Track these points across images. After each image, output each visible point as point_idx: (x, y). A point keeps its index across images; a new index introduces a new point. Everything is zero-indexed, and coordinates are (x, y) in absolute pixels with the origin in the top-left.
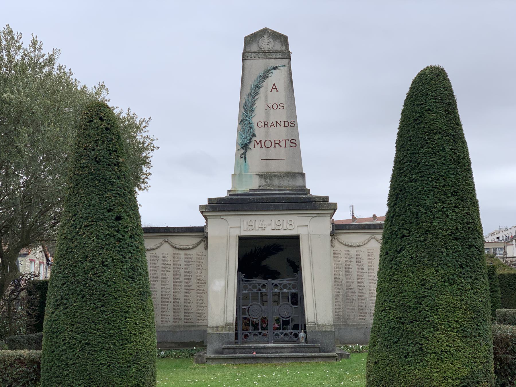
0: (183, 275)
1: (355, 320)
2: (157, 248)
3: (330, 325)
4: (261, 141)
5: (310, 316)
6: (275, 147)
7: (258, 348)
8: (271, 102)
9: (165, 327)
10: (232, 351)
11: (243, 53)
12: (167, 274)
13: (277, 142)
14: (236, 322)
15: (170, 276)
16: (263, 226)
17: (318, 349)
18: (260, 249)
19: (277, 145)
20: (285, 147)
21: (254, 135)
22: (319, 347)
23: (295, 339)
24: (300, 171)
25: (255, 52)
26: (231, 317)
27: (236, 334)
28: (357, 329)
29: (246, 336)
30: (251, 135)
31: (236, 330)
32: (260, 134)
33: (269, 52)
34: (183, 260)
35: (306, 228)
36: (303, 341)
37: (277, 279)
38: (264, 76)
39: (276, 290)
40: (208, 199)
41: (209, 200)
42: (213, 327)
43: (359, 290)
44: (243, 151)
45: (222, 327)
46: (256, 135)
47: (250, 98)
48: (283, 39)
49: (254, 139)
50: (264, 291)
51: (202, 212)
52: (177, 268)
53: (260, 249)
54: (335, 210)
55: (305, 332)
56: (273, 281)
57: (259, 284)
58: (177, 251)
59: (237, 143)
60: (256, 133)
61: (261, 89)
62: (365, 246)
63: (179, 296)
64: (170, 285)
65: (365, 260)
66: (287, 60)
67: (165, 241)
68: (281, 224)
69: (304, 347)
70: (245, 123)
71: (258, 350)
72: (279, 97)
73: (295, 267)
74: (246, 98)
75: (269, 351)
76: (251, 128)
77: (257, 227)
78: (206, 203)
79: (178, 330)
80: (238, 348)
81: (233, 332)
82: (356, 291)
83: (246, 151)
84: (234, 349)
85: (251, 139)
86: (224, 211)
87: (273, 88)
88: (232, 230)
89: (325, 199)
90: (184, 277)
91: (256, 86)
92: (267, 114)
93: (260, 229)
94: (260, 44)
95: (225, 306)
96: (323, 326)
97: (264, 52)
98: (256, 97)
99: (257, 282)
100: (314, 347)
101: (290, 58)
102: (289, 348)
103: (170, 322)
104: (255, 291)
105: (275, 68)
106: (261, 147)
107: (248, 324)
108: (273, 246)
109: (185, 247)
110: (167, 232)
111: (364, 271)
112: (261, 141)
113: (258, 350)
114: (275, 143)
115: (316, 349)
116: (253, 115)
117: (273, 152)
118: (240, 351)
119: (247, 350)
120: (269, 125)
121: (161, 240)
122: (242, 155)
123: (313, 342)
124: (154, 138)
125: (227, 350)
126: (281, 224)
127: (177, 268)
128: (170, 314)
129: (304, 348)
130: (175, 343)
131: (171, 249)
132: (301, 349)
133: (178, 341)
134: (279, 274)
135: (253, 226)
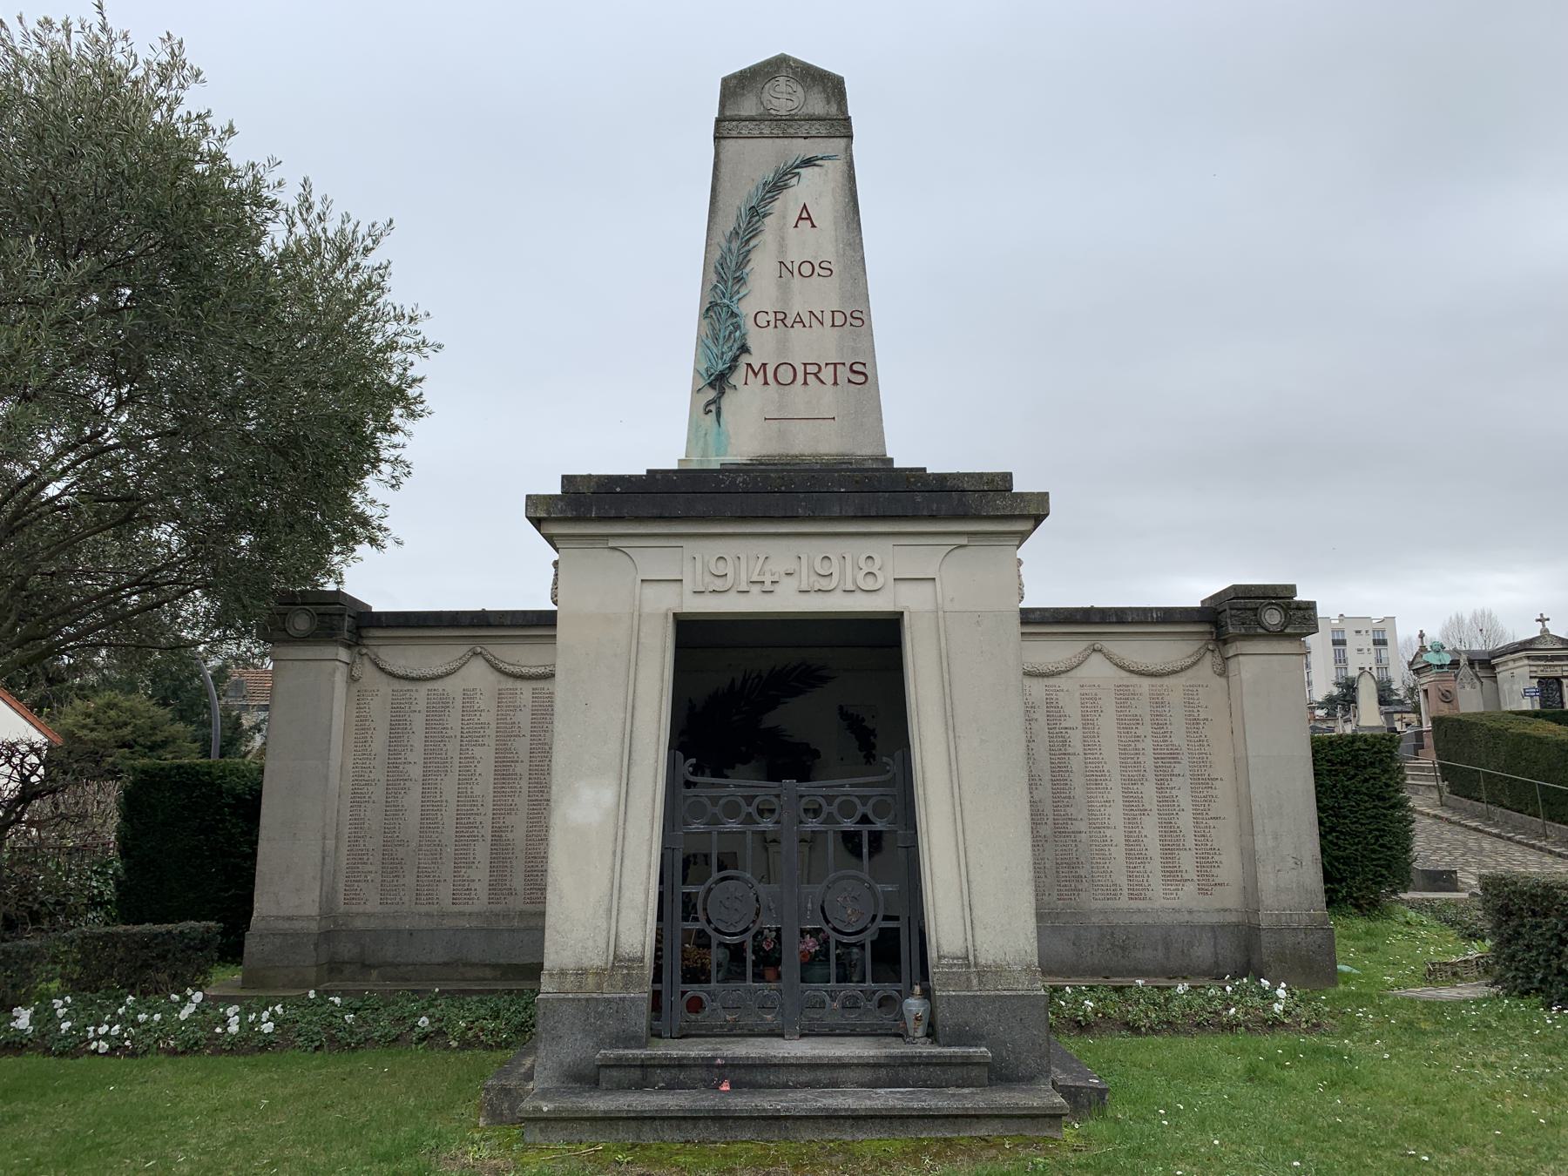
0: (524, 754)
2: (447, 674)
5: (944, 930)
6: (805, 383)
8: (794, 256)
9: (462, 914)
10: (636, 1074)
11: (718, 121)
12: (478, 752)
14: (657, 958)
15: (485, 757)
16: (768, 579)
18: (759, 676)
19: (810, 378)
20: (835, 383)
21: (744, 349)
23: (887, 1019)
24: (876, 451)
25: (752, 119)
26: (638, 932)
27: (656, 995)
29: (695, 1005)
31: (657, 978)
32: (763, 346)
33: (791, 119)
36: (920, 1033)
37: (808, 780)
38: (777, 186)
39: (812, 824)
41: (567, 480)
42: (563, 973)
44: (711, 394)
45: (599, 973)
47: (735, 245)
48: (833, 87)
49: (745, 359)
50: (767, 824)
51: (537, 522)
52: (507, 733)
53: (759, 676)
54: (1038, 519)
55: (927, 994)
56: (803, 788)
57: (749, 799)
58: (510, 684)
59: (696, 371)
60: (750, 343)
61: (766, 220)
63: (509, 820)
64: (484, 786)
65: (1074, 717)
66: (842, 142)
67: (475, 654)
68: (835, 570)
69: (929, 1062)
70: (720, 313)
71: (747, 1075)
72: (821, 243)
74: (724, 244)
75: (783, 1078)
76: (737, 327)
77: (744, 577)
78: (556, 490)
79: (504, 924)
80: (661, 1066)
81: (642, 993)
82: (1049, 810)
83: (722, 393)
84: (644, 1065)
85: (735, 359)
86: (619, 519)
87: (800, 218)
88: (650, 590)
89: (1002, 482)
91: (754, 211)
92: (784, 290)
93: (755, 589)
94: (766, 96)
95: (616, 889)
96: (998, 971)
97: (777, 120)
98: (752, 243)
100: (967, 1062)
101: (851, 137)
102: (867, 1065)
103: (480, 900)
104: (733, 825)
105: (808, 162)
106: (766, 383)
107: (704, 952)
108: (795, 668)
109: (533, 670)
110: (479, 626)
111: (1070, 750)
116: (743, 291)
117: (800, 398)
118: (667, 1075)
119: (698, 1074)
120: (789, 322)
121: (462, 650)
122: (708, 404)
123: (960, 1038)
124: (420, 312)
126: (835, 570)
127: (507, 733)
128: (480, 876)
130: (495, 966)
131: (493, 677)
132: (914, 1071)
133: (501, 961)
134: (816, 754)
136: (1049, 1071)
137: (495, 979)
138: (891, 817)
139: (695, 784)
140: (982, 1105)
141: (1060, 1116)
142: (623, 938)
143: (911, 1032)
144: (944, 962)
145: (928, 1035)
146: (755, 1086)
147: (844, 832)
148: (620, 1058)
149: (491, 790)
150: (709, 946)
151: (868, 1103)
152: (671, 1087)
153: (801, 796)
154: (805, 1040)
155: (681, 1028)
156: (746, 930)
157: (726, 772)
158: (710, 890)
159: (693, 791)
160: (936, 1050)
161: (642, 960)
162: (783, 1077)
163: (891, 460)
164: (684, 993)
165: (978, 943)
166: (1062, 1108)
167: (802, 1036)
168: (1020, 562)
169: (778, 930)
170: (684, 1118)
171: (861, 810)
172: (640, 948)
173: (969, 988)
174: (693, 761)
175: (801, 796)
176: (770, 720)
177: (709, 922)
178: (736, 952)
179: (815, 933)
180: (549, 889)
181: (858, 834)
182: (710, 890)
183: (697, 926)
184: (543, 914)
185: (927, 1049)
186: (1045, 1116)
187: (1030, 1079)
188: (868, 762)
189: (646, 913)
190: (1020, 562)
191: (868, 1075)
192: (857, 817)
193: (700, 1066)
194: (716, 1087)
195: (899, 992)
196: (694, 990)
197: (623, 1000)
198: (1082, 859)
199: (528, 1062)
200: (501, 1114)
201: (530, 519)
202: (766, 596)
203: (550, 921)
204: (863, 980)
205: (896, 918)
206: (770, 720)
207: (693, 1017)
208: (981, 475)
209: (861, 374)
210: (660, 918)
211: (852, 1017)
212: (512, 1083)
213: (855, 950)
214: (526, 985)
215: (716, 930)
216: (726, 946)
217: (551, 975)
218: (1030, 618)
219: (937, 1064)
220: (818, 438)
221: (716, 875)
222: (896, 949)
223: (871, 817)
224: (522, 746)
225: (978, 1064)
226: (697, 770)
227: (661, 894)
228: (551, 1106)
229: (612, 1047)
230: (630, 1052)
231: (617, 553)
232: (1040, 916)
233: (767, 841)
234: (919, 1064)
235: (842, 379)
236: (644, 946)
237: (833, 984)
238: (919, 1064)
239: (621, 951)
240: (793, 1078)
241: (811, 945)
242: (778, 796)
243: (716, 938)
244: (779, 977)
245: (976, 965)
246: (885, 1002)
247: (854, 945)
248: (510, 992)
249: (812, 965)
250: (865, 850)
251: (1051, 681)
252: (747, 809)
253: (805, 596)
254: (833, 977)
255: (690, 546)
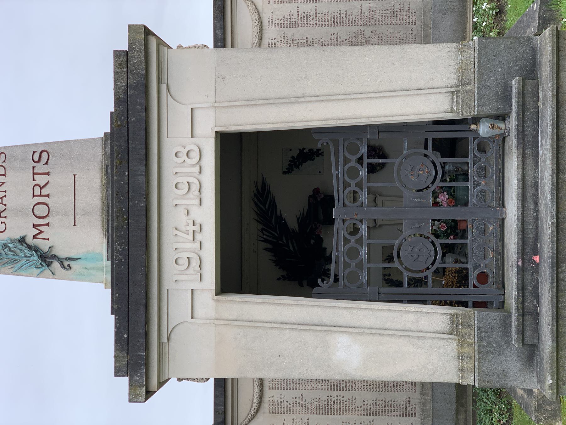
1: (414, 33)
3: (461, 51)
4: (34, 226)
5: (432, 106)
6: (48, 196)
7: (523, 249)
10: (529, 320)
13: (37, 192)
14: (451, 304)
16: (191, 228)
17: (529, 82)
19: (44, 192)
20: (48, 174)
21: (22, 240)
22: (523, 81)
23: (492, 148)
26: (433, 318)
27: (476, 305)
28: (434, 28)
29: (483, 278)
30: (20, 247)
31: (464, 304)
34: (285, 392)
35: (198, 115)
36: (502, 125)
37: (333, 197)
39: (363, 197)
40: (116, 375)
41: (118, 372)
42: (461, 370)
43: (353, 24)
44: (56, 265)
45: (461, 344)
46: (23, 235)
49: (29, 240)
50: (363, 229)
51: (149, 394)
54: (148, 32)
55: (476, 120)
56: (338, 204)
57: (346, 241)
58: (265, 405)
59: (38, 275)
60: (18, 236)
62: (260, 9)
63: (359, 403)
69: (522, 121)
73: (302, 149)
77: (189, 245)
79: (429, 406)
80: (523, 303)
81: (475, 315)
82: (355, 29)
83: (55, 257)
84: (523, 313)
85: (29, 247)
88: (199, 312)
89: (122, 59)
90: (320, 392)
93: (199, 237)
95: (404, 333)
96: (462, 71)
99: (341, 248)
100: (522, 94)
104: (363, 253)
106: (48, 225)
107: (450, 273)
108: (256, 204)
111: (313, 13)
112: (34, 226)
113: (529, 249)
114: (41, 195)
115: (529, 89)
117: (59, 199)
119: (528, 278)
122: (64, 267)
123: (506, 98)
125: (528, 333)
129: (523, 121)
130: (457, 412)
131: (260, 418)
132: (528, 130)
133: (454, 407)
134: (316, 191)
135: (190, 255)
136: (529, 38)
137: (466, 412)
138: (358, 143)
139: (336, 276)
140: (550, 85)
141: (558, 32)
142: (439, 328)
143: (502, 132)
144: (455, 109)
145: (504, 120)
146: (537, 238)
147: (369, 172)
148: (518, 331)
149: (339, 416)
150: (444, 269)
151: (549, 162)
152: (537, 296)
153: (344, 205)
154: (506, 204)
155: (498, 288)
156: (432, 242)
157: (328, 254)
158: (406, 268)
159: (340, 278)
160: (514, 115)
161: (452, 315)
162: (530, 219)
163: (105, 134)
164: (475, 286)
165: (443, 85)
166: (553, 30)
167: (503, 206)
168: (180, 47)
169: (432, 220)
170: (557, 287)
171: (353, 163)
172: (444, 317)
173: (473, 92)
174: (319, 280)
175: (344, 205)
176: (292, 223)
177: (428, 269)
178: (448, 249)
179: (435, 195)
180: (405, 379)
181: (369, 165)
182: (406, 268)
183: (430, 277)
184: (423, 384)
185: (513, 121)
186: (558, 43)
187: (534, 51)
188: (322, 154)
189: (421, 313)
190: (180, 47)
191: (530, 162)
192: (359, 166)
193: (523, 275)
194: (537, 265)
195: (475, 139)
196: (472, 279)
197: (479, 328)
198: (388, 7)
199: (520, 392)
200: (554, 410)
201: (146, 399)
202: (204, 228)
203: (427, 379)
204: (468, 163)
205: (426, 140)
206: (292, 223)
207: (490, 280)
208: (116, 73)
209: (41, 156)
210: (424, 302)
211: (491, 171)
212: (534, 403)
213: (447, 167)
214: (470, 393)
215: (433, 264)
216: (444, 255)
217: (462, 378)
218: (221, 40)
219: (523, 115)
220: (90, 187)
221: (396, 264)
222: (447, 141)
223: (359, 156)
224: (309, 396)
225: (523, 87)
226: (326, 274)
227: (409, 302)
228: (549, 378)
229: (510, 336)
230: (514, 324)
231: (173, 336)
232: (426, 39)
233: (374, 226)
234: (523, 126)
235: (45, 169)
236: (443, 314)
237: (469, 185)
238: (523, 126)
239: (447, 329)
240: (531, 213)
241: (443, 198)
242: (344, 221)
243: (438, 265)
244: (465, 221)
245: (457, 86)
246: (482, 148)
247: (443, 168)
248: (475, 402)
249: (458, 199)
250: (381, 161)
251: (265, 24)
252: (353, 243)
253: (204, 202)
254: (464, 184)
255: (168, 283)
